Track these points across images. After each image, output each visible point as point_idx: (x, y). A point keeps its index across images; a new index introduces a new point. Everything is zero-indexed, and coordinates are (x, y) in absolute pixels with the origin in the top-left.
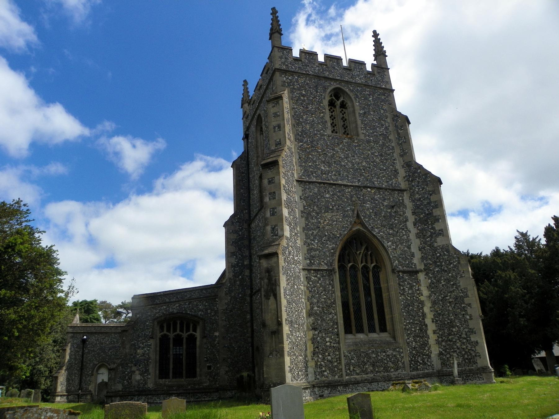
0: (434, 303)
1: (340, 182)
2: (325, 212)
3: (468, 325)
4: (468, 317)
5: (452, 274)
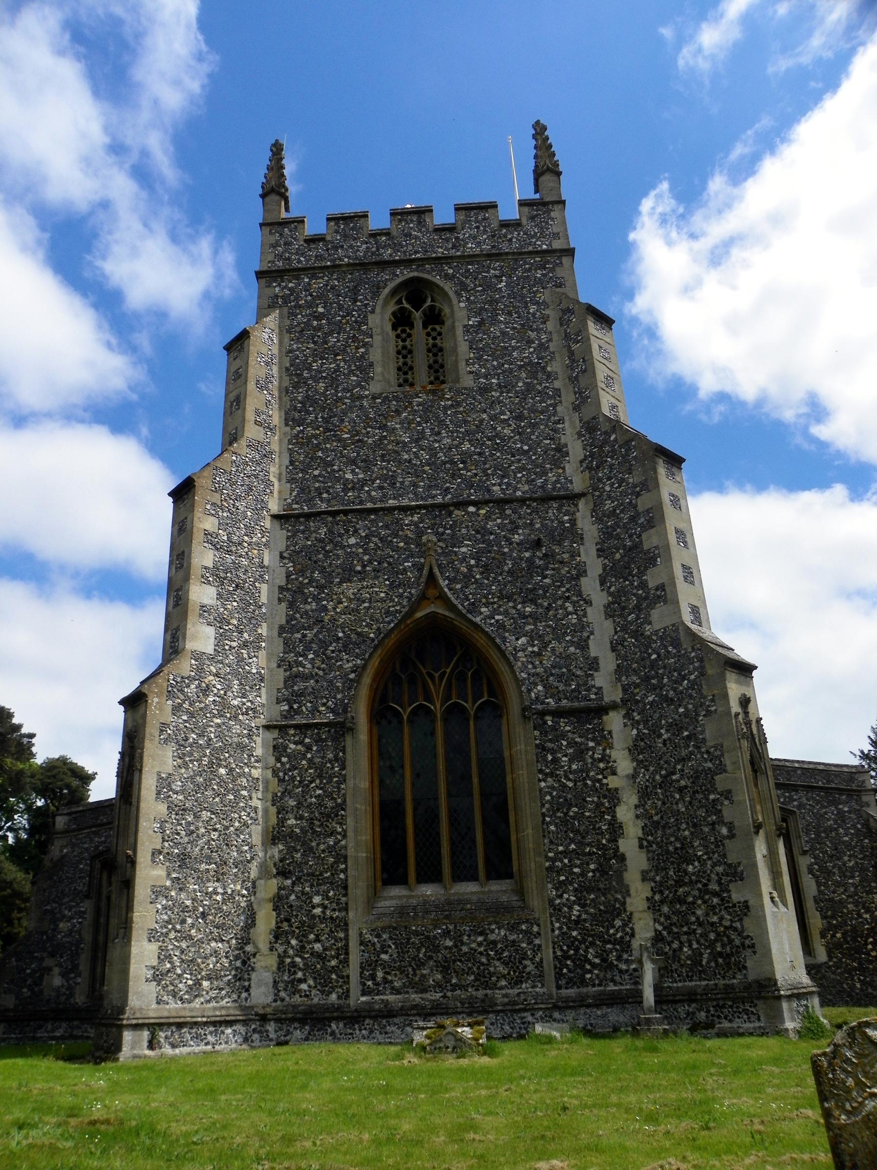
0: (644, 794)
1: (392, 502)
2: (340, 583)
3: (725, 856)
4: (724, 831)
5: (686, 708)
